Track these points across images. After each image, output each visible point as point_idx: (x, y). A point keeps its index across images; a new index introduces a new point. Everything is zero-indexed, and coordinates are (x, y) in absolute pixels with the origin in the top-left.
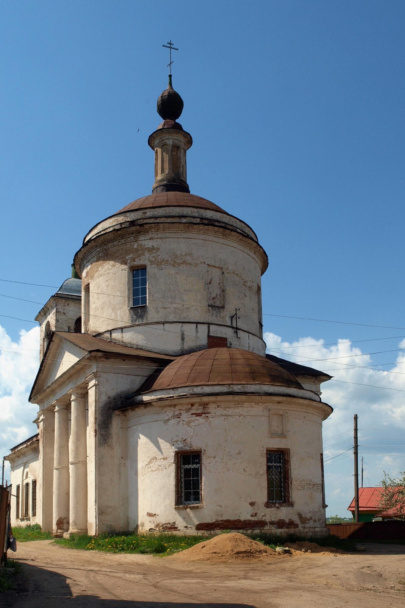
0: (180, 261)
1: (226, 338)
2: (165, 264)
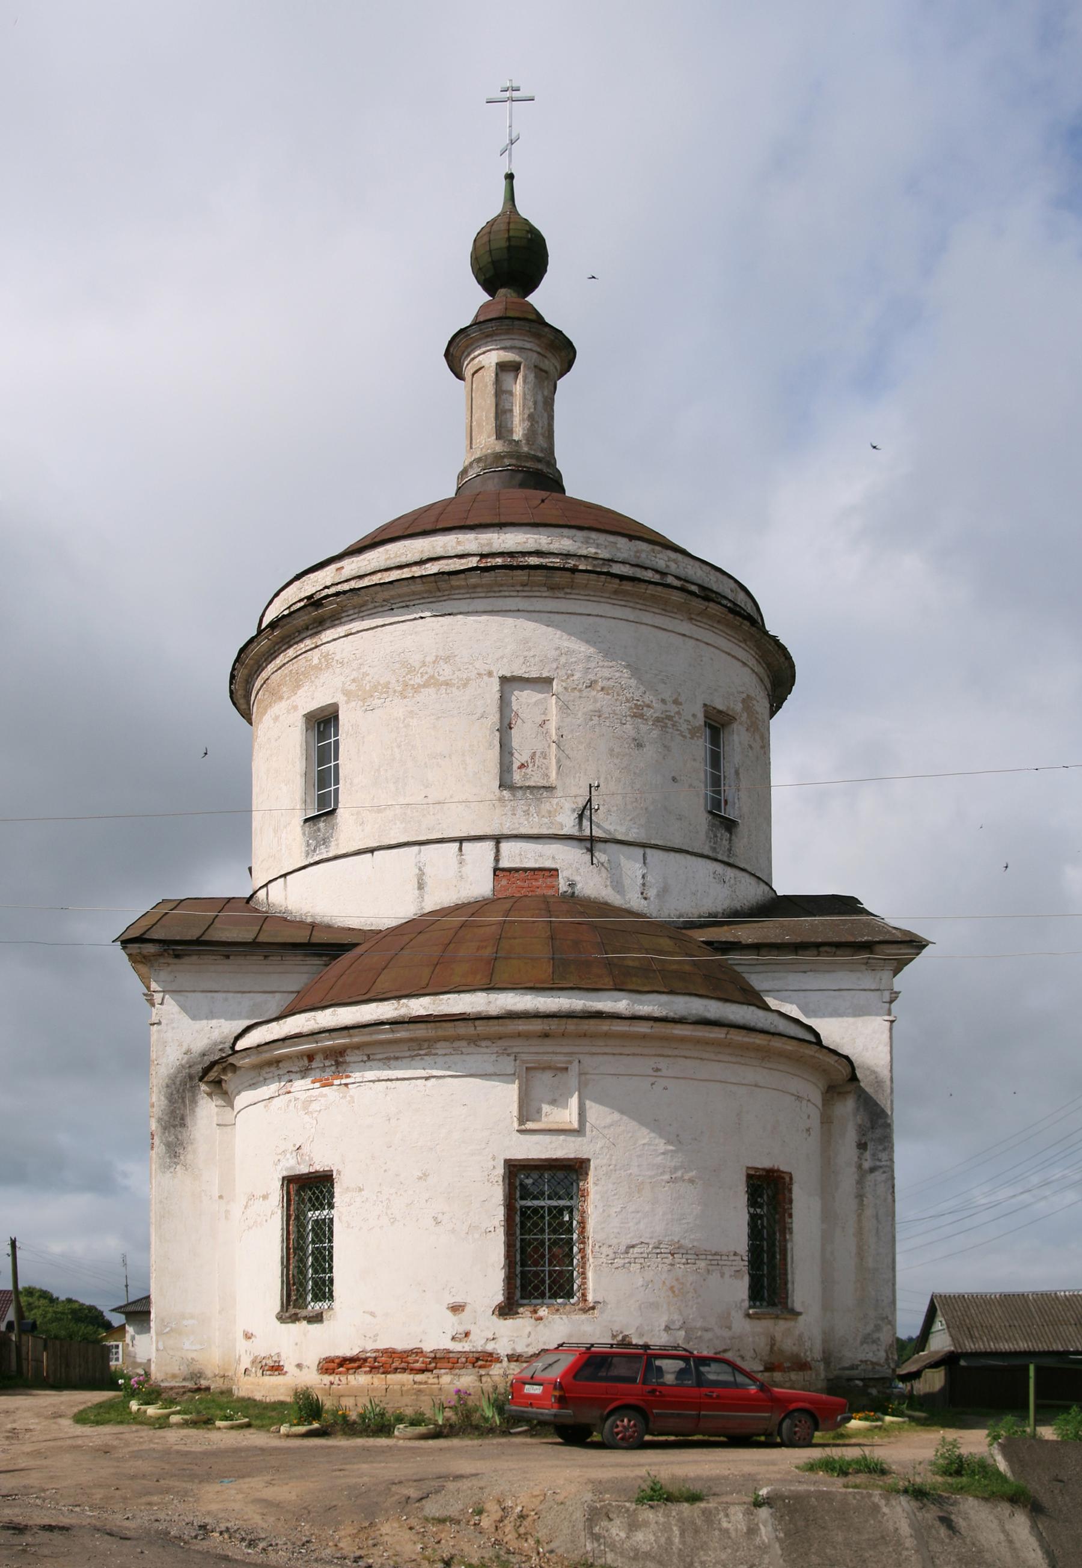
0: (418, 680)
1: (556, 870)
2: (381, 693)
